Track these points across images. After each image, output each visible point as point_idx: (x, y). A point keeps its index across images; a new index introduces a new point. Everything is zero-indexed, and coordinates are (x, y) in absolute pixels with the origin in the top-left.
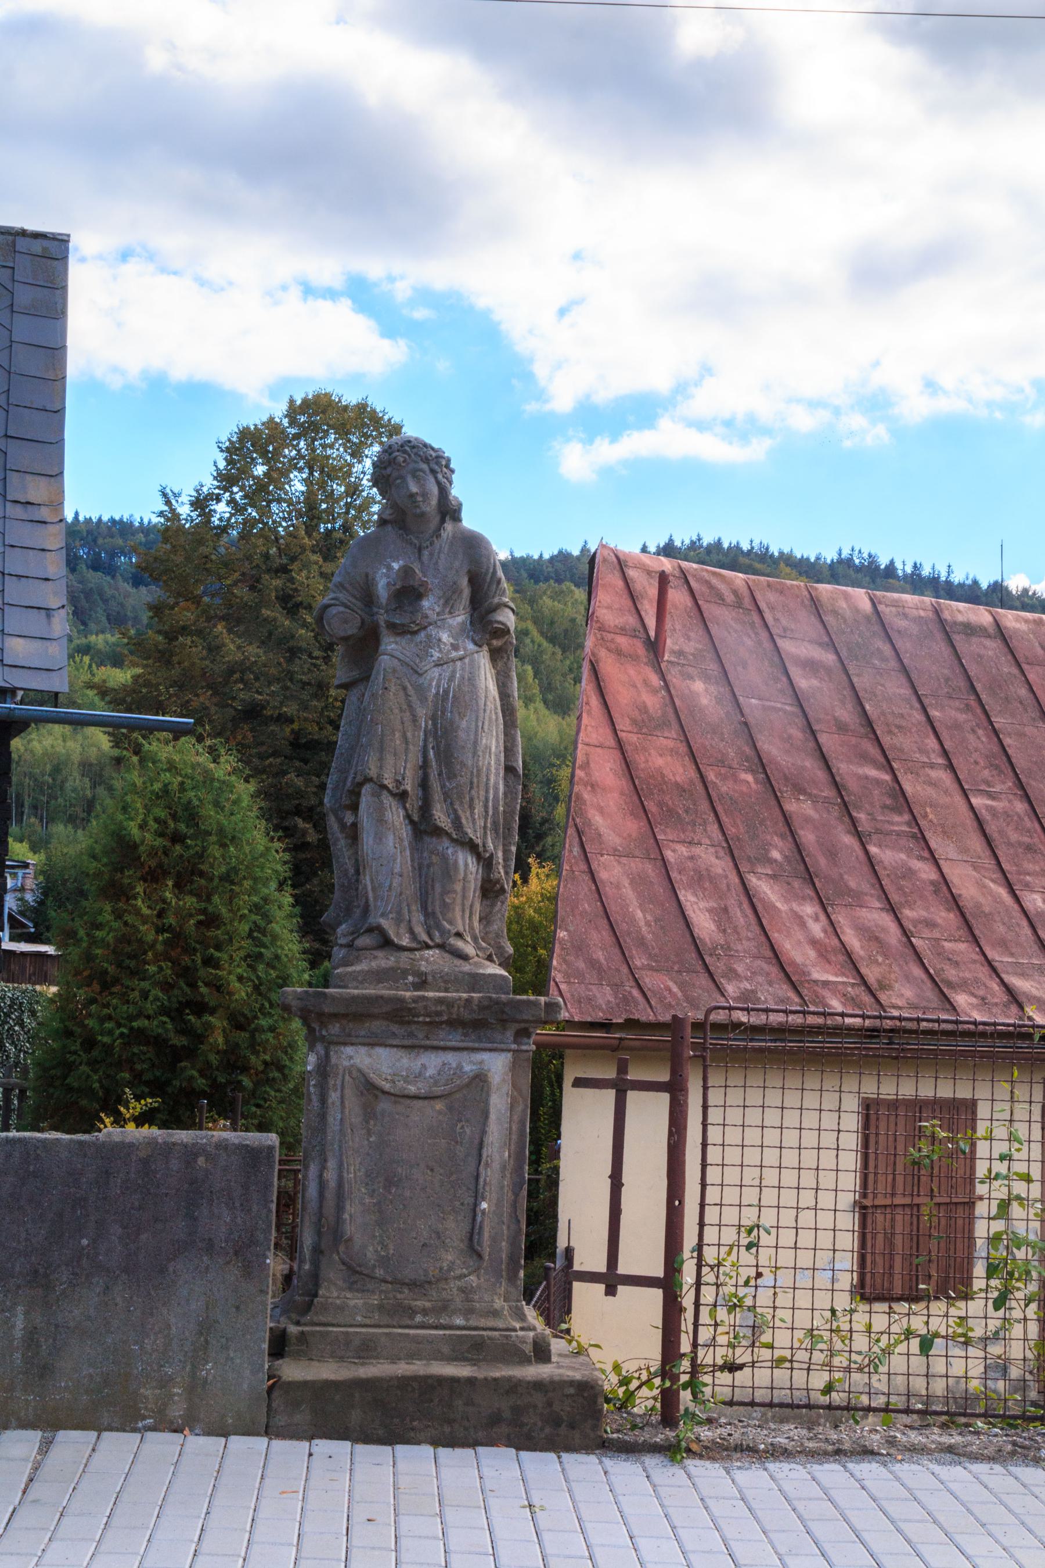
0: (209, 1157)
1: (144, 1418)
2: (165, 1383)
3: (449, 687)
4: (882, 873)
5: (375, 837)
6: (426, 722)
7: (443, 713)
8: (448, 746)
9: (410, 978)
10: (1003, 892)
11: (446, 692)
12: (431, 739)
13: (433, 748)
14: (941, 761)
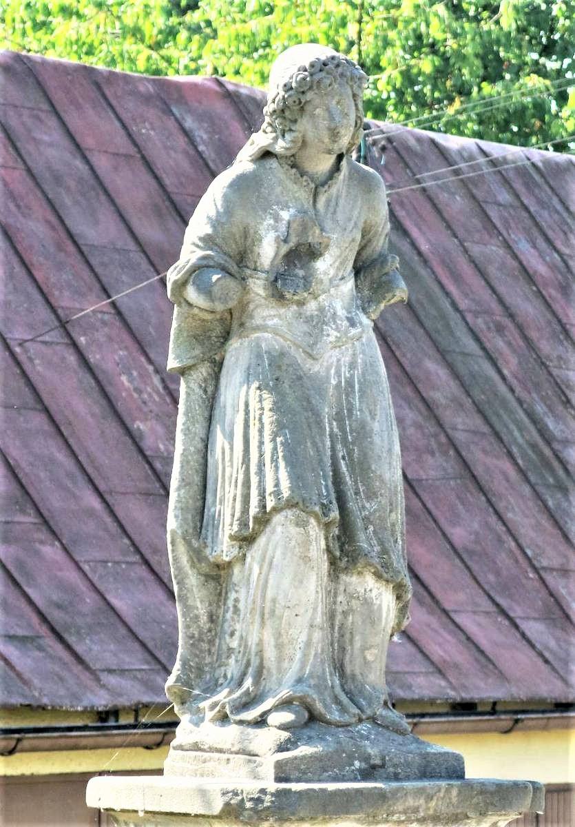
3: (352, 376)
5: (294, 579)
6: (331, 424)
7: (350, 411)
8: (364, 455)
9: (357, 764)
11: (350, 383)
12: (339, 446)
13: (344, 458)
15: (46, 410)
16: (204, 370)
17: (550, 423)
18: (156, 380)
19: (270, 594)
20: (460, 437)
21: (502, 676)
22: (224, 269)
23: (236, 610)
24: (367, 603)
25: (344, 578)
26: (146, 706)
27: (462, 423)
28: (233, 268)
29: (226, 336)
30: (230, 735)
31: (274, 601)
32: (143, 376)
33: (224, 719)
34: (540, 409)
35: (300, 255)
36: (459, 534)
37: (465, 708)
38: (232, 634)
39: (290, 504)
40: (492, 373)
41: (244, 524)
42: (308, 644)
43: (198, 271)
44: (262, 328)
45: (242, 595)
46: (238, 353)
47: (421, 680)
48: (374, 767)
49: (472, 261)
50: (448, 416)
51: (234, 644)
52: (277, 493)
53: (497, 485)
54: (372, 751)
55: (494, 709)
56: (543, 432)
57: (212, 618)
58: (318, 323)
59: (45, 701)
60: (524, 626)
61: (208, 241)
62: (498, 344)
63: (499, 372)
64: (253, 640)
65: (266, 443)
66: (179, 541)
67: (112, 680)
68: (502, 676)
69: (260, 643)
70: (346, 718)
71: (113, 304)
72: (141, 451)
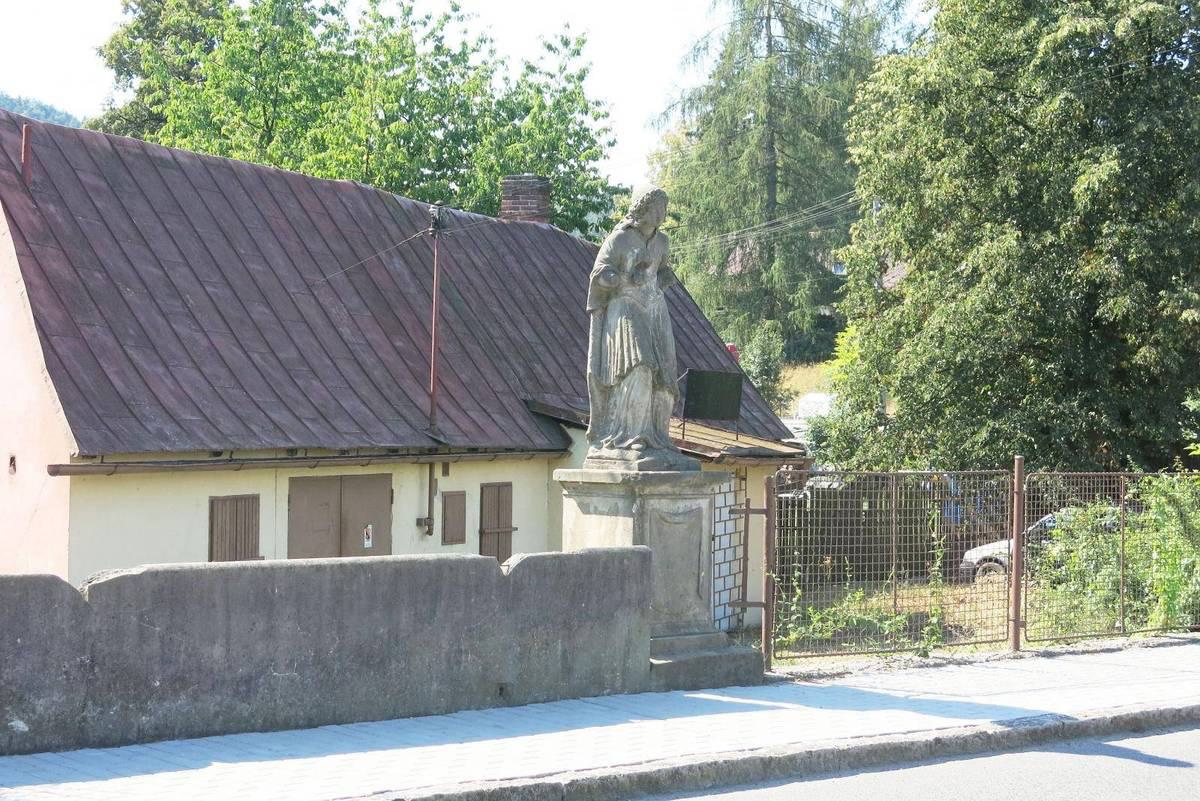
0: (629, 559)
1: (606, 688)
2: (613, 671)
4: (185, 342)
7: (659, 327)
10: (239, 352)
11: (658, 316)
14: (180, 260)
15: (306, 322)
16: (600, 311)
17: (491, 329)
18: (345, 310)
19: (631, 399)
20: (460, 336)
21: (489, 438)
22: (614, 272)
23: (615, 405)
24: (665, 402)
25: (657, 392)
26: (361, 448)
27: (460, 329)
28: (616, 270)
29: (608, 298)
30: (615, 453)
31: (633, 401)
32: (340, 309)
33: (612, 447)
34: (487, 324)
35: (641, 266)
36: (463, 376)
37: (474, 450)
38: (612, 414)
39: (642, 364)
40: (467, 307)
41: (622, 370)
42: (646, 417)
43: (604, 273)
44: (626, 294)
45: (620, 400)
46: (615, 304)
47: (459, 438)
48: (671, 466)
49: (455, 261)
50: (454, 327)
51: (614, 418)
52: (637, 359)
53: (476, 357)
54: (670, 459)
55: (486, 451)
56: (489, 333)
57: (603, 408)
58: (646, 293)
59: (326, 445)
60: (493, 416)
61: (606, 261)
62: (468, 295)
63: (470, 307)
64: (622, 417)
65: (630, 340)
66: (593, 380)
67: (347, 437)
68: (489, 438)
69: (626, 418)
70: (660, 446)
71: (325, 277)
72: (342, 339)
